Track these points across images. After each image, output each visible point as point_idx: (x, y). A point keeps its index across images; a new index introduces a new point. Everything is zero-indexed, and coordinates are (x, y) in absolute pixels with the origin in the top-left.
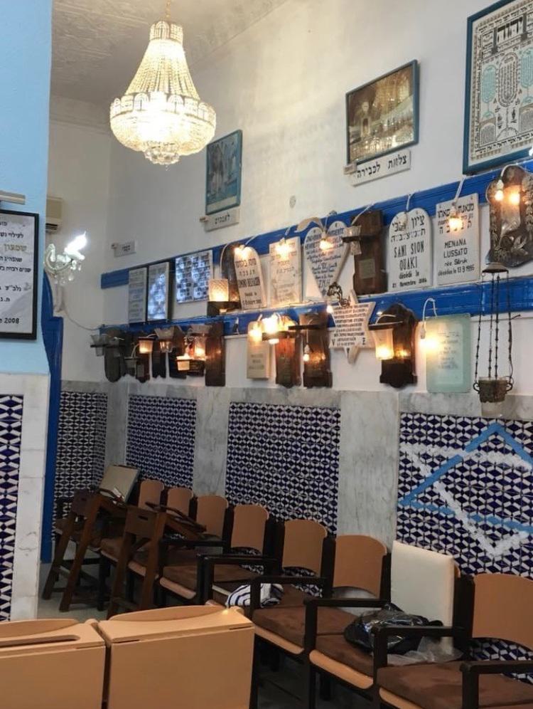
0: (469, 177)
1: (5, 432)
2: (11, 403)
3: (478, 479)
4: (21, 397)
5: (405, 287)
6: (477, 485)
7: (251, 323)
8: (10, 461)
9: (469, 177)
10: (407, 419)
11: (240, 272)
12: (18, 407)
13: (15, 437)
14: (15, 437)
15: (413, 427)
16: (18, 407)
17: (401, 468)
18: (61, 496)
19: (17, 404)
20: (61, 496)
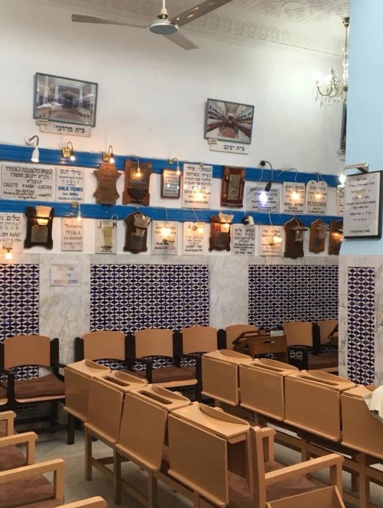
0: (79, 212)
1: (3, 292)
2: (34, 268)
3: (361, 275)
4: (38, 265)
5: (255, 209)
6: (361, 278)
7: (335, 238)
8: (5, 329)
9: (79, 212)
10: (352, 271)
11: (7, 220)
12: (37, 284)
13: (36, 327)
14: (36, 327)
15: (357, 275)
16: (37, 284)
17: (374, 285)
18: (31, 378)
19: (36, 268)
20: (31, 378)
